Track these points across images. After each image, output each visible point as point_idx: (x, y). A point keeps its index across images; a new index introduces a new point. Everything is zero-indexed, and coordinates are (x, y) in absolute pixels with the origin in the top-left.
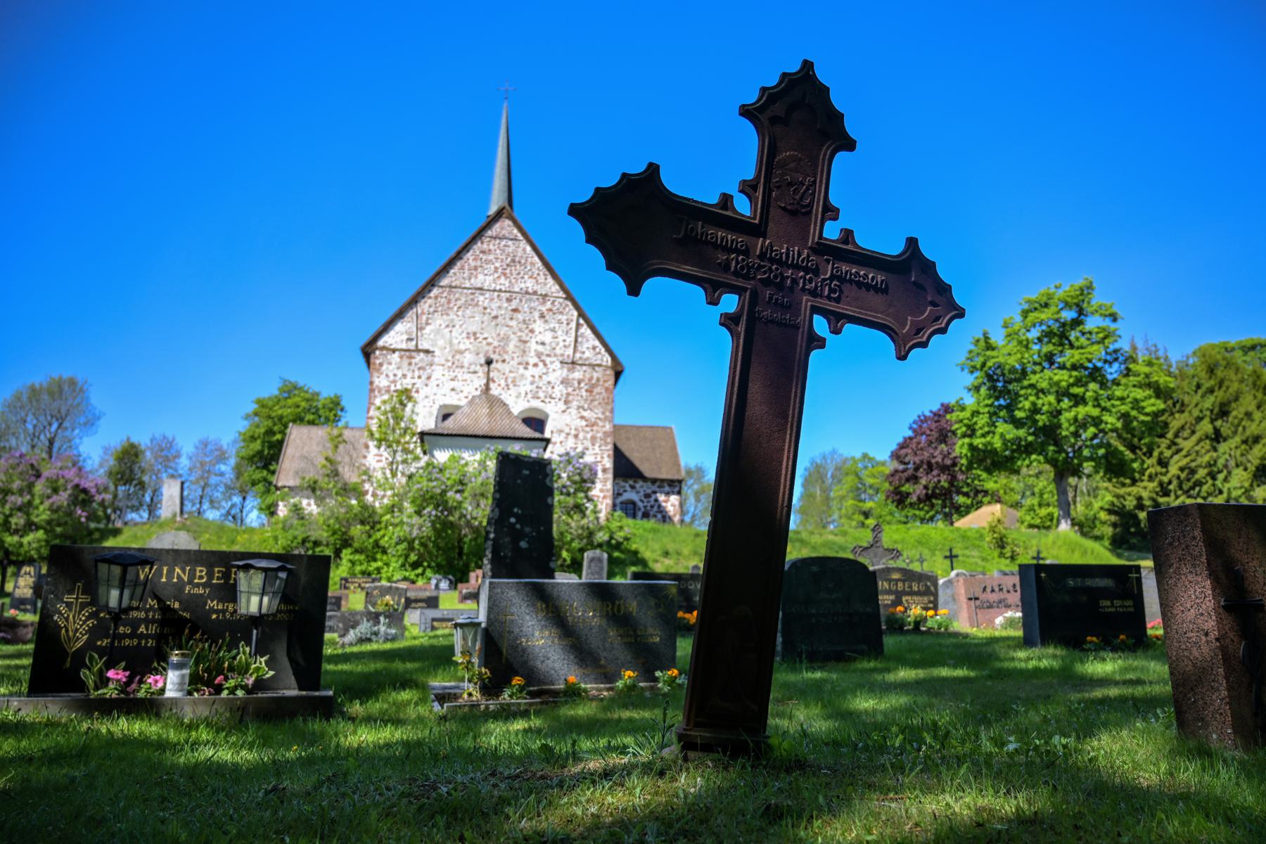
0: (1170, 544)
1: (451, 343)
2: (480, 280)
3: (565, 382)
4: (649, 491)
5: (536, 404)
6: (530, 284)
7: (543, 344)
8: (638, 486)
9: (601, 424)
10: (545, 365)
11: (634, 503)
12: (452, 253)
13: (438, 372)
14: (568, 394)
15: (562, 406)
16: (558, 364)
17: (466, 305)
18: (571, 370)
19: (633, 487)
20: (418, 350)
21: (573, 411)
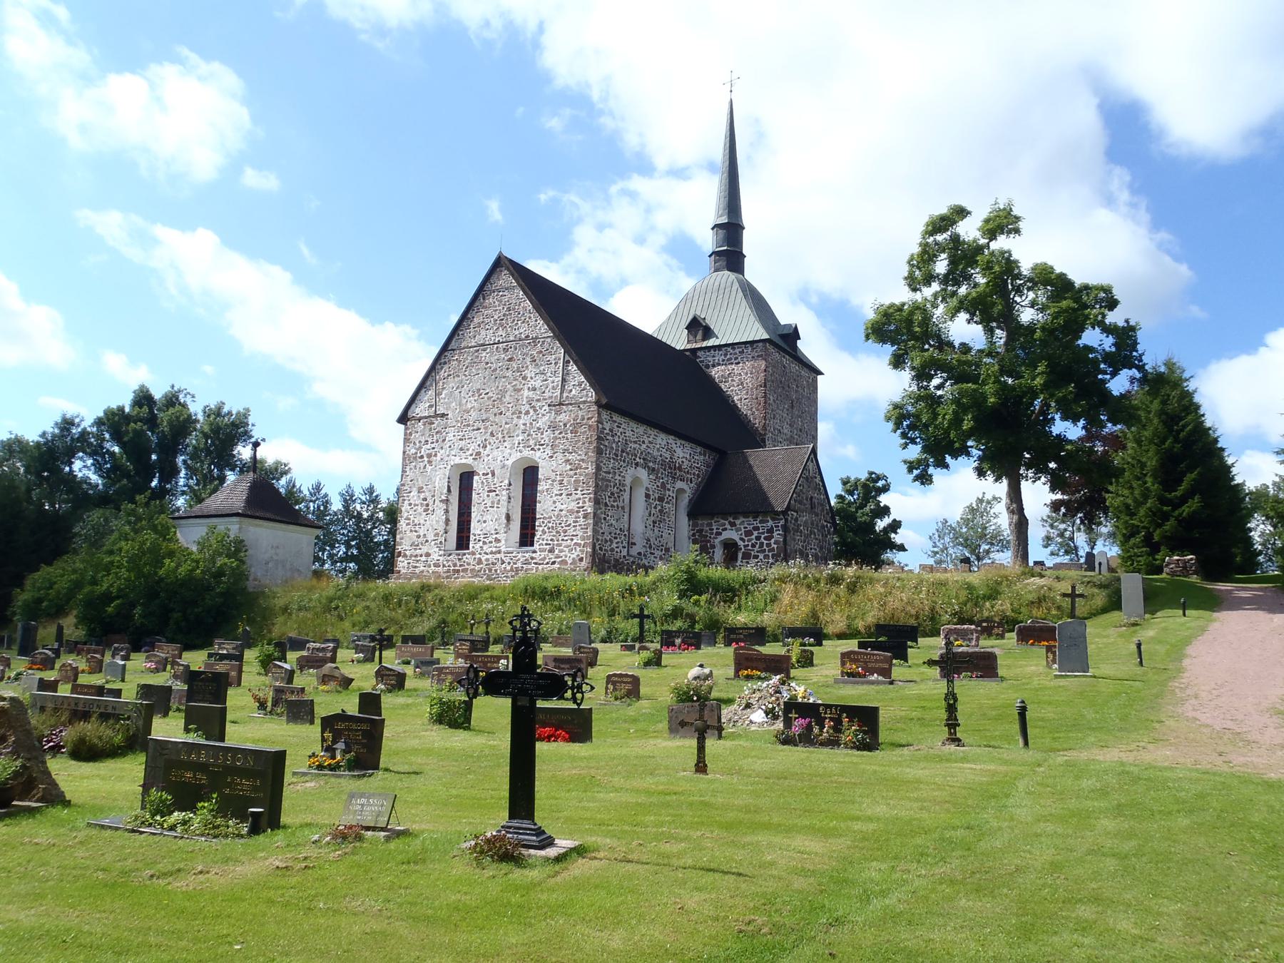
0: (581, 560)
1: (460, 405)
2: (479, 339)
3: (553, 427)
4: (750, 528)
5: (527, 453)
6: (523, 330)
7: (534, 389)
8: (738, 522)
9: (584, 465)
10: (535, 411)
11: (735, 544)
12: (454, 319)
13: (451, 435)
14: (555, 438)
15: (549, 451)
16: (546, 407)
17: (473, 363)
18: (558, 413)
19: (732, 524)
20: (436, 416)
21: (560, 456)
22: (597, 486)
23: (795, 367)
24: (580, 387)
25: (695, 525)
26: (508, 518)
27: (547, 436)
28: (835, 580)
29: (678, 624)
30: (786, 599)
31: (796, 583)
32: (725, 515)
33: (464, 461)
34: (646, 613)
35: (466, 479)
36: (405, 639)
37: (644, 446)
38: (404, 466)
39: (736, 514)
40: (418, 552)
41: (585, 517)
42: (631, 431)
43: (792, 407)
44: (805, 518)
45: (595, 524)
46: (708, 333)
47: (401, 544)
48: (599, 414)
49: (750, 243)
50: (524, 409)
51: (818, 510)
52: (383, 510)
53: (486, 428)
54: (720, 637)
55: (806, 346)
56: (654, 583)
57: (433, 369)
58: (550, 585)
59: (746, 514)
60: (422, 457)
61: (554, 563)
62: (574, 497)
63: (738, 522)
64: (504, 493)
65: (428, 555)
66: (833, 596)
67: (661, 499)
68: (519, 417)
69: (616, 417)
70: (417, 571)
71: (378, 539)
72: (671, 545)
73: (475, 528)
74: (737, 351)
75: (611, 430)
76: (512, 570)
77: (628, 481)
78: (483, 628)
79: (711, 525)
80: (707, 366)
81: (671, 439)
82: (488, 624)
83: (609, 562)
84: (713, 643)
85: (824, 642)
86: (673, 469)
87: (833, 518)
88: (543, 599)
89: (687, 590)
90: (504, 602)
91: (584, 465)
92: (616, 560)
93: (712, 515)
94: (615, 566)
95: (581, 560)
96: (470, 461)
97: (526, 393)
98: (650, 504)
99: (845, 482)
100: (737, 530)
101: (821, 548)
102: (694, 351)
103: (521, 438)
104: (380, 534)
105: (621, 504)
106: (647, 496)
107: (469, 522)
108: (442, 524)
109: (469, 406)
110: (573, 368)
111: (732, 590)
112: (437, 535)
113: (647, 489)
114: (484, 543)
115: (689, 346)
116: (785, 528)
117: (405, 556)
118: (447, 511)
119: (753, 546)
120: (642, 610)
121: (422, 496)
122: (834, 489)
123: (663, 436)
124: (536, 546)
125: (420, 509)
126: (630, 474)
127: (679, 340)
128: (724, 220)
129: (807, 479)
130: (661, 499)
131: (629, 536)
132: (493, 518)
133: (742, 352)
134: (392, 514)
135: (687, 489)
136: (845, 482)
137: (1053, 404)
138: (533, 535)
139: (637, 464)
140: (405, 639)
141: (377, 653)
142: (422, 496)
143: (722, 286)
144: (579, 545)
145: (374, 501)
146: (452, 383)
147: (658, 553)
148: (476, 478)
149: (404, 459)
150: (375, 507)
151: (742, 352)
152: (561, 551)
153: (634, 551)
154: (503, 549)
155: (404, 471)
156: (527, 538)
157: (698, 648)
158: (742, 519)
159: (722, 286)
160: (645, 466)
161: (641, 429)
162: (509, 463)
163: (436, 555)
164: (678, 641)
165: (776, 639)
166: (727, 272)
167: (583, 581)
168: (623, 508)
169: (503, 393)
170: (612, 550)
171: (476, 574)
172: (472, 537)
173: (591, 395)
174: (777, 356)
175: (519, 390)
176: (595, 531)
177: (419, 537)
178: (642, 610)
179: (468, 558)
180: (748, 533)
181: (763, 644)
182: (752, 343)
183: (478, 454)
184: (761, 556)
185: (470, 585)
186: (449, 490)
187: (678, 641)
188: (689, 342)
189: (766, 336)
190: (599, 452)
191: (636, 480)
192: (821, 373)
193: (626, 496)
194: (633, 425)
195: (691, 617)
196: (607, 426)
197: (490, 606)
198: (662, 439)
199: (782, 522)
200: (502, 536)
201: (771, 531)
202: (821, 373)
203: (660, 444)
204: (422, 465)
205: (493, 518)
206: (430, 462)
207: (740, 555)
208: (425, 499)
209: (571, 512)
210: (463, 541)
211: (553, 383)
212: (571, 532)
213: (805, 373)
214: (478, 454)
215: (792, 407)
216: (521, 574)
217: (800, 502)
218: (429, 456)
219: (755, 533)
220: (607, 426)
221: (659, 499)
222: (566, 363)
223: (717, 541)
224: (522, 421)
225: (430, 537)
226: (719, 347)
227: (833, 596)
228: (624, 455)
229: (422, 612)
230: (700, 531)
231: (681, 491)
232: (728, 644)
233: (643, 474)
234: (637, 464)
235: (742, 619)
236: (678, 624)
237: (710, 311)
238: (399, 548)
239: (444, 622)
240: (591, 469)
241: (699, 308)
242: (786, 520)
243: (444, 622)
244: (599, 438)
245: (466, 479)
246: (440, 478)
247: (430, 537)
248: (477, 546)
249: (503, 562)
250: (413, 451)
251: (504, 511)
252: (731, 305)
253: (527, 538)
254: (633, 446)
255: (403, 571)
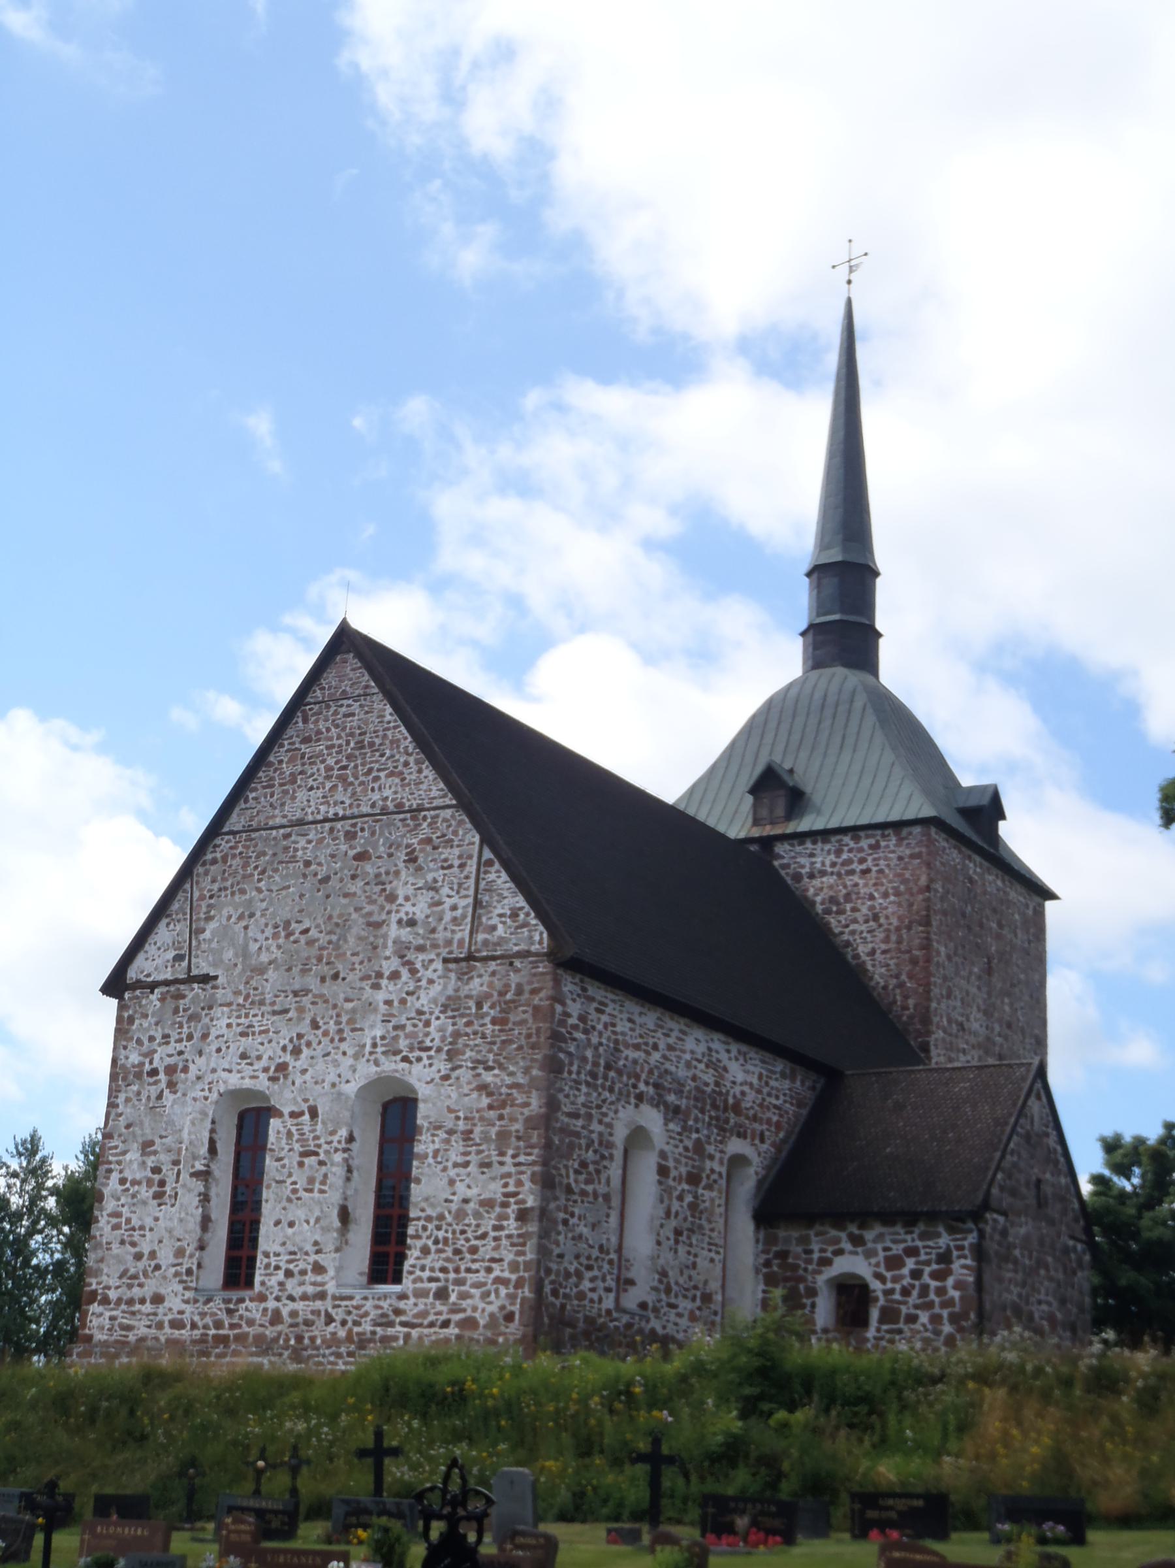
0: (509, 1317)
2: (293, 811)
4: (897, 1249)
5: (391, 1066)
6: (389, 791)
7: (412, 923)
9: (520, 1099)
10: (413, 972)
13: (221, 1022)
14: (457, 1035)
15: (443, 1066)
16: (438, 965)
18: (464, 977)
20: (191, 979)
22: (548, 1146)
23: (994, 882)
24: (512, 920)
25: (770, 1241)
26: (345, 1215)
27: (439, 1028)
28: (1105, 1382)
29: (740, 1480)
30: (993, 1425)
31: (1014, 1389)
32: (839, 1219)
33: (248, 1083)
34: (665, 1450)
35: (251, 1121)
36: (103, 1506)
37: (656, 1056)
38: (113, 1092)
39: (864, 1218)
40: (136, 1292)
41: (523, 1216)
42: (625, 1024)
43: (989, 971)
44: (1023, 1229)
45: (544, 1234)
46: (796, 800)
47: (97, 1273)
48: (557, 982)
49: (895, 611)
50: (387, 967)
51: (1054, 1210)
52: (55, 1191)
53: (301, 1010)
54: (841, 1512)
55: (1019, 835)
56: (684, 1379)
57: (186, 873)
58: (442, 1377)
59: (888, 1218)
60: (154, 1072)
61: (446, 1324)
62: (498, 1170)
63: (869, 1235)
64: (338, 1157)
65: (158, 1299)
66: (1105, 1421)
67: (693, 1179)
68: (376, 987)
69: (596, 991)
70: (132, 1338)
71: (42, 1259)
72: (714, 1286)
73: (269, 1239)
74: (864, 843)
75: (583, 1018)
76: (349, 1338)
77: (620, 1135)
78: (282, 1480)
79: (804, 1240)
80: (798, 877)
81: (717, 1043)
82: (295, 1471)
83: (572, 1324)
84: (821, 1529)
85: (1092, 1536)
86: (722, 1112)
87: (1088, 1231)
88: (424, 1416)
89: (761, 1397)
90: (334, 1418)
91: (520, 1099)
92: (590, 1321)
93: (809, 1218)
94: (587, 1334)
95: (509, 1317)
96: (262, 1083)
97: (393, 931)
98: (668, 1191)
99: (1111, 1146)
100: (869, 1254)
101: (1063, 1301)
102: (767, 843)
103: (378, 1033)
104: (46, 1250)
105: (602, 1189)
106: (663, 1171)
107: (255, 1224)
108: (194, 1223)
109: (264, 958)
110: (499, 878)
111: (866, 1399)
112: (180, 1253)
113: (663, 1155)
114: (289, 1274)
115: (756, 832)
116: (979, 1253)
117: (106, 1301)
118: (205, 1198)
119: (906, 1292)
120: (656, 1442)
121: (151, 1162)
122: (1088, 1163)
123: (698, 1033)
124: (407, 1284)
125: (145, 1193)
126: (623, 1120)
127: (735, 821)
128: (835, 555)
129: (1027, 1137)
130: (693, 1179)
131: (621, 1261)
132: (309, 1224)
133: (875, 847)
134: (79, 1202)
135: (757, 1154)
136: (1111, 1146)
137: (670, 1419)
138: (401, 1258)
139: (640, 1097)
140: (103, 1506)
141: (39, 1540)
142: (151, 1162)
143: (831, 699)
144: (504, 1282)
145: (37, 1171)
146: (228, 910)
147: (685, 1305)
148: (274, 1123)
149: (114, 1077)
150: (40, 1186)
151: (875, 847)
152: (464, 1296)
153: (630, 1301)
154: (331, 1288)
155: (111, 1105)
156: (386, 1264)
157: (789, 1540)
158: (878, 1229)
159: (831, 699)
160: (658, 1102)
161: (650, 1018)
162: (351, 1089)
163: (175, 1301)
164: (742, 1522)
165: (971, 1522)
166: (840, 671)
167: (517, 1370)
168: (607, 1198)
169: (340, 926)
170: (581, 1296)
171: (265, 1345)
172: (261, 1261)
173: (538, 937)
174: (953, 855)
175: (378, 925)
176: (543, 1251)
177: (138, 1257)
178: (656, 1442)
179: (251, 1309)
180: (894, 1263)
181: (943, 1536)
182: (898, 826)
183: (282, 1067)
184: (924, 1317)
185: (252, 1376)
186: (212, 1150)
187: (742, 1522)
188: (756, 822)
189: (928, 812)
190: (554, 1067)
191: (638, 1137)
192: (1052, 896)
193: (614, 1171)
194: (633, 1007)
195: (770, 1462)
196: (575, 1008)
197: (301, 1426)
198: (697, 1042)
199: (972, 1238)
200: (328, 1260)
201: (945, 1258)
202: (1052, 896)
203: (691, 1051)
204: (153, 1091)
205: (309, 1224)
206: (172, 1085)
207: (875, 1314)
208: (156, 1170)
209: (488, 1204)
210: (239, 1269)
211: (455, 896)
212: (487, 1250)
213: (1016, 894)
214: (282, 1067)
215: (989, 971)
216: (372, 1351)
217: (1014, 1193)
218: (171, 1070)
219: (910, 1263)
220: (575, 1008)
221: (688, 1178)
222: (483, 866)
223: (821, 1280)
224: (381, 996)
225: (166, 1256)
226: (824, 835)
227: (1105, 1421)
228: (614, 1076)
229: (143, 1438)
230: (783, 1255)
231: (738, 1161)
232: (861, 1531)
233: (652, 1119)
234: (640, 1097)
235: (887, 1471)
236: (740, 1480)
237: (803, 755)
238: (93, 1284)
239: (193, 1462)
240: (536, 1103)
241: (780, 748)
242: (981, 1234)
243: (193, 1462)
244: (556, 1038)
245: (251, 1121)
246: (190, 1119)
247: (166, 1256)
248: (273, 1282)
249: (330, 1320)
250: (134, 1058)
251: (334, 1197)
252: (850, 741)
253: (386, 1264)
254: (632, 1054)
255: (99, 1337)
